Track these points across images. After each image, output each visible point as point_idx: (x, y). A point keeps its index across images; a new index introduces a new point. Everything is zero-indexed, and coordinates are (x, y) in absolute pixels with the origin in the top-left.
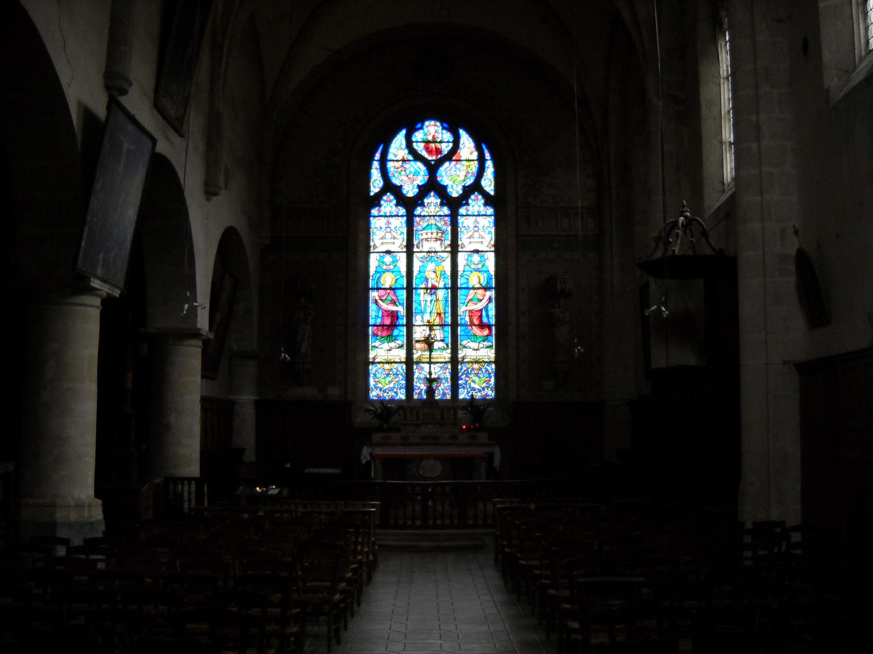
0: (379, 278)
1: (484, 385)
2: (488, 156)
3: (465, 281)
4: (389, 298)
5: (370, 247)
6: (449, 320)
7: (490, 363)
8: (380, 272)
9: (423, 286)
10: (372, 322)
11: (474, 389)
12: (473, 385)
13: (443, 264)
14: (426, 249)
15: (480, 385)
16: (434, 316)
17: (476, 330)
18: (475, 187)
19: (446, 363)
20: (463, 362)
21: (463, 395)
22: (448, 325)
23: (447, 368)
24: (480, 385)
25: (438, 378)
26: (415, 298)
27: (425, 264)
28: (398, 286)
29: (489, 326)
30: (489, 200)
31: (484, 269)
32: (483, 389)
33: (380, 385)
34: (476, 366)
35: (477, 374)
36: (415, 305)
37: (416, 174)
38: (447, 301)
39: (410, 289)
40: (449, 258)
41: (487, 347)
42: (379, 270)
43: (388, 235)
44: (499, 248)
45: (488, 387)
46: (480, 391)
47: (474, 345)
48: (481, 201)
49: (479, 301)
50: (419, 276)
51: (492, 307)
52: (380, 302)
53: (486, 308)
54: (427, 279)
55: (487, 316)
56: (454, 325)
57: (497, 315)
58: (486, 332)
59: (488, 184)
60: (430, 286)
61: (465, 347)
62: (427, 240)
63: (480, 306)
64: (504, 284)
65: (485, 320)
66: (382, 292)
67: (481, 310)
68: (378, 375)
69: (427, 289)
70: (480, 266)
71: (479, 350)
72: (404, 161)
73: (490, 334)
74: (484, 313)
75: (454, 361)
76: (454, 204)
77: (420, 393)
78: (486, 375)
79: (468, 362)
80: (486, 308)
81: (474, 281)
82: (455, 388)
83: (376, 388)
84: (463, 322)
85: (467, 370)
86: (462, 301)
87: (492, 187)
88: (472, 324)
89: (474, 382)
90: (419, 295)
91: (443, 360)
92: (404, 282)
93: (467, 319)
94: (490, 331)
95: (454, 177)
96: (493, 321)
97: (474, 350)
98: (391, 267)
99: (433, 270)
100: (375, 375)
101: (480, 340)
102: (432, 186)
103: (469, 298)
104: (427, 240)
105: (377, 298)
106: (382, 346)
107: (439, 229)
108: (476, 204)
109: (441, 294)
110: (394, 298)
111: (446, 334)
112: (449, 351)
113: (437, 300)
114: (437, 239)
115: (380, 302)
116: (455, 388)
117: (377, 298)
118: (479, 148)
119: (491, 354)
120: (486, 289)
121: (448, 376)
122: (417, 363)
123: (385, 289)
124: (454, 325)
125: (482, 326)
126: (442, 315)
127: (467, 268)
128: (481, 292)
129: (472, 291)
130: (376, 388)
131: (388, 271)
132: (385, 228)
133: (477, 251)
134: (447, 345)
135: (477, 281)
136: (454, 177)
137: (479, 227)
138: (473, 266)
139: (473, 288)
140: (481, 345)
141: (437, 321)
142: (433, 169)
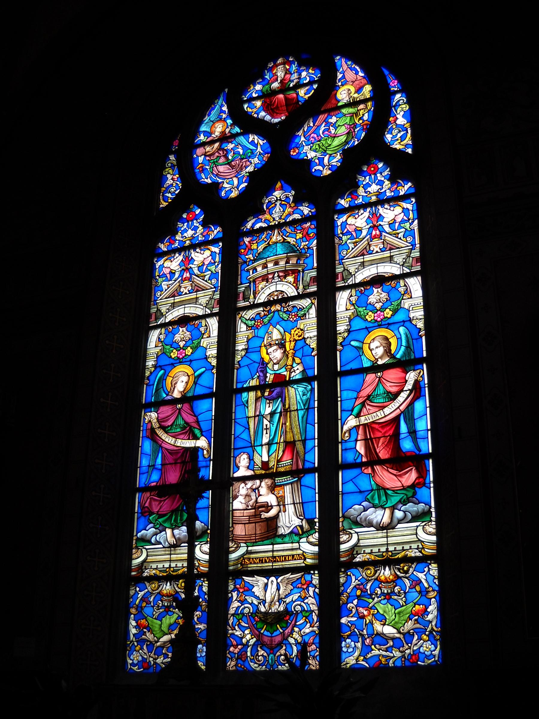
0: (163, 379)
1: (410, 625)
2: (394, 85)
3: (355, 353)
4: (180, 422)
5: (149, 315)
6: (314, 458)
7: (424, 560)
8: (166, 365)
9: (254, 383)
10: (141, 481)
11: (382, 638)
12: (378, 627)
13: (301, 324)
14: (262, 298)
15: (397, 626)
16: (278, 450)
17: (387, 478)
18: (367, 150)
19: (307, 569)
20: (350, 565)
21: (351, 655)
22: (312, 470)
23: (309, 583)
24: (397, 626)
25: (287, 612)
26: (238, 413)
27: (261, 332)
28: (199, 391)
29: (417, 460)
30: (400, 166)
31: (400, 316)
32: (408, 636)
33: (149, 636)
34: (386, 573)
35: (388, 597)
36: (237, 430)
37: (247, 156)
38: (308, 409)
39: (226, 393)
40: (313, 312)
41: (414, 519)
42: (164, 361)
43: (186, 286)
44: (431, 266)
45: (420, 632)
46: (397, 643)
47: (380, 516)
48: (383, 172)
49: (396, 402)
50: (246, 361)
51: (422, 406)
52: (160, 433)
53: (408, 413)
54: (263, 365)
55: (413, 433)
56: (330, 467)
57: (436, 429)
58: (412, 476)
59: (399, 137)
60: (270, 378)
61: (358, 524)
62: (265, 278)
63: (391, 410)
64: (450, 350)
65: (407, 445)
66: (166, 410)
67: (396, 420)
68: (148, 611)
69: (261, 387)
70: (388, 313)
71: (396, 527)
72: (224, 138)
73: (420, 483)
74: (404, 428)
75: (331, 564)
76: (325, 195)
77: (241, 656)
78: (414, 595)
79: (364, 564)
80: (408, 413)
81: (374, 350)
82: (331, 633)
83: (142, 642)
84: (350, 457)
85: (361, 586)
86: (348, 405)
87: (408, 140)
88: (373, 461)
89: (383, 621)
90: (246, 405)
91: (299, 563)
92: (210, 381)
93: (360, 447)
94: (422, 473)
95: (322, 146)
96: (427, 446)
97: (380, 528)
98: (189, 351)
99: (277, 345)
100: (140, 609)
101: (395, 500)
102: (283, 168)
103: (364, 393)
104: (265, 278)
105: (156, 425)
106: (160, 537)
107: (292, 249)
108: (375, 183)
109: (296, 394)
110: (190, 419)
111: (308, 494)
112: (315, 537)
113: (286, 411)
114: (286, 273)
115: (160, 433)
116: (331, 633)
117: (156, 425)
118: (374, 77)
119: (427, 535)
120: (405, 364)
121: (312, 603)
122: (239, 574)
123: (175, 401)
124: (330, 467)
125: (399, 461)
126: (299, 446)
127: (358, 324)
128: (393, 374)
129: (370, 377)
130: (142, 642)
131: (180, 361)
132: (184, 277)
133: (378, 281)
134: (311, 522)
135: (380, 351)
136: (322, 146)
137: (383, 234)
138: (370, 317)
139: (375, 368)
140: (399, 514)
141: (287, 463)
142: (280, 139)
